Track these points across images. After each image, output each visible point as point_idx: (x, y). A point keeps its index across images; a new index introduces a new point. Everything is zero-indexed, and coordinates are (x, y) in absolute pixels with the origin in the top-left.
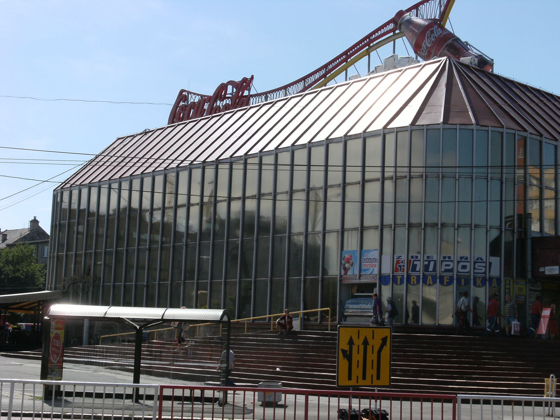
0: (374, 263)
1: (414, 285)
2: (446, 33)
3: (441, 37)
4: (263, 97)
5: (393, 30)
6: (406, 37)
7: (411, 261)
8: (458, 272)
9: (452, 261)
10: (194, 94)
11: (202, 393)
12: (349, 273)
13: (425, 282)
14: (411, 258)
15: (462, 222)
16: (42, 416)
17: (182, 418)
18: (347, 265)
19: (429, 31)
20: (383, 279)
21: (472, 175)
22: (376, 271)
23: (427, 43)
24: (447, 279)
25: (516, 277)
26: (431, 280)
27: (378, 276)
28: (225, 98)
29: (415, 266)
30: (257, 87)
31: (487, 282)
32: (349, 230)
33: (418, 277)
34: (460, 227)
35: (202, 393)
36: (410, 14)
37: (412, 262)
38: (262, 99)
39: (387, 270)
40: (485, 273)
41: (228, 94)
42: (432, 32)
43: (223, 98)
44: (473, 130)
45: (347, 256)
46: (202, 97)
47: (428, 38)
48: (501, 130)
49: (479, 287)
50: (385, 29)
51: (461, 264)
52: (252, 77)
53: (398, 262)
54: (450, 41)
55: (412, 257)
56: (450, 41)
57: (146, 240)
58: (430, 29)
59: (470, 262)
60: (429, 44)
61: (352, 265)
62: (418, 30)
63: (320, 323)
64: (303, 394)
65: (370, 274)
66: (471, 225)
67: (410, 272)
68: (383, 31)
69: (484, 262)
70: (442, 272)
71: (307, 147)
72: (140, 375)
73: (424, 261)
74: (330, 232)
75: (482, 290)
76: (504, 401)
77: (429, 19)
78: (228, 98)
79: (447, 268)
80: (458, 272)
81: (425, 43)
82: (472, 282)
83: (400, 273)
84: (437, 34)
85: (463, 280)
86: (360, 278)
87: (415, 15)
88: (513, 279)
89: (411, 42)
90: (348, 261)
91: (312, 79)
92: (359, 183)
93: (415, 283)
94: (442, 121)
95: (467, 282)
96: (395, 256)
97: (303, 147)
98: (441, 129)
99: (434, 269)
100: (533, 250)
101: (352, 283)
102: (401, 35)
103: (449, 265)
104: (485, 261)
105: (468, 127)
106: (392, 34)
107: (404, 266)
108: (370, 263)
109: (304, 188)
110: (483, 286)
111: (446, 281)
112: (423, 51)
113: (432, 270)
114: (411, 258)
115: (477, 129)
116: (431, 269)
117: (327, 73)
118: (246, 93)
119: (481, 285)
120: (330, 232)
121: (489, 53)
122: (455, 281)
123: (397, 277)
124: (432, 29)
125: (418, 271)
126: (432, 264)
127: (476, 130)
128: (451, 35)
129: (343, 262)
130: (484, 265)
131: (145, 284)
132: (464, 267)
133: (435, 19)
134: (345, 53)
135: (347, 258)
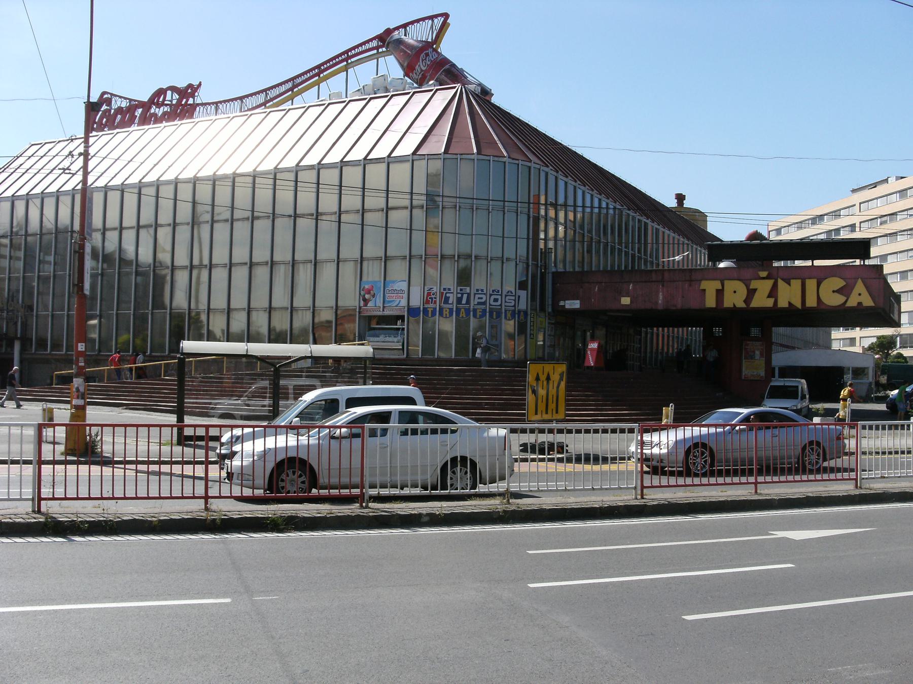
0: (401, 295)
1: (446, 317)
2: (441, 57)
3: (438, 61)
4: (213, 107)
5: (377, 48)
6: (394, 55)
7: (443, 293)
8: (490, 305)
9: (484, 294)
10: (121, 97)
11: (207, 432)
12: (370, 304)
13: (441, 314)
14: (444, 290)
15: (494, 255)
16: (21, 462)
17: (171, 459)
18: (367, 296)
19: (422, 55)
20: (413, 312)
21: (517, 210)
22: (404, 303)
23: (421, 66)
24: (480, 312)
25: (539, 311)
26: (464, 313)
27: (406, 308)
28: (163, 104)
29: (447, 299)
30: (203, 96)
31: (517, 316)
32: (369, 259)
33: (451, 310)
34: (492, 259)
35: (207, 432)
36: (399, 33)
37: (444, 294)
38: (207, 110)
39: (416, 302)
40: (514, 306)
41: (167, 100)
42: (427, 55)
43: (159, 105)
44: (505, 162)
45: (367, 287)
46: (130, 102)
47: (423, 60)
48: (529, 164)
49: (509, 320)
50: (367, 46)
51: (493, 297)
52: (200, 84)
53: (429, 294)
54: (447, 67)
55: (445, 289)
56: (447, 67)
57: (49, 263)
58: (425, 52)
59: (501, 295)
60: (425, 67)
61: (374, 296)
62: (411, 51)
63: (150, 354)
64: (193, 427)
65: (396, 306)
66: (470, 256)
67: (442, 304)
68: (360, 49)
69: (513, 296)
70: (475, 305)
71: (317, 168)
72: (185, 416)
73: (457, 293)
74: (345, 261)
75: (512, 322)
76: (530, 429)
77: (425, 41)
78: (167, 105)
79: (480, 300)
80: (490, 305)
81: (419, 66)
82: (503, 314)
83: (431, 305)
84: (432, 57)
85: (495, 313)
86: (383, 310)
87: (403, 34)
88: (537, 312)
89: (402, 63)
90: (368, 292)
91: (277, 91)
92: (383, 210)
93: (448, 316)
94: (443, 151)
95: (499, 315)
96: (426, 287)
97: (311, 168)
98: (476, 160)
99: (468, 302)
100: (554, 284)
101: (374, 315)
102: (388, 53)
103: (482, 298)
104: (485, 292)
105: (469, 157)
106: (375, 51)
107: (435, 298)
108: (396, 295)
109: (312, 213)
110: (512, 319)
111: (478, 314)
112: (416, 74)
113: (465, 303)
114: (444, 290)
115: (510, 162)
116: (464, 301)
117: (295, 86)
118: (191, 101)
119: (510, 318)
120: (345, 261)
121: (488, 84)
122: (488, 314)
123: (428, 309)
124: (427, 52)
125: (450, 304)
126: (465, 296)
127: (477, 159)
128: (445, 61)
129: (362, 293)
130: (513, 298)
131: (98, 314)
132: (496, 300)
133: (427, 42)
134: (318, 67)
135: (367, 289)
